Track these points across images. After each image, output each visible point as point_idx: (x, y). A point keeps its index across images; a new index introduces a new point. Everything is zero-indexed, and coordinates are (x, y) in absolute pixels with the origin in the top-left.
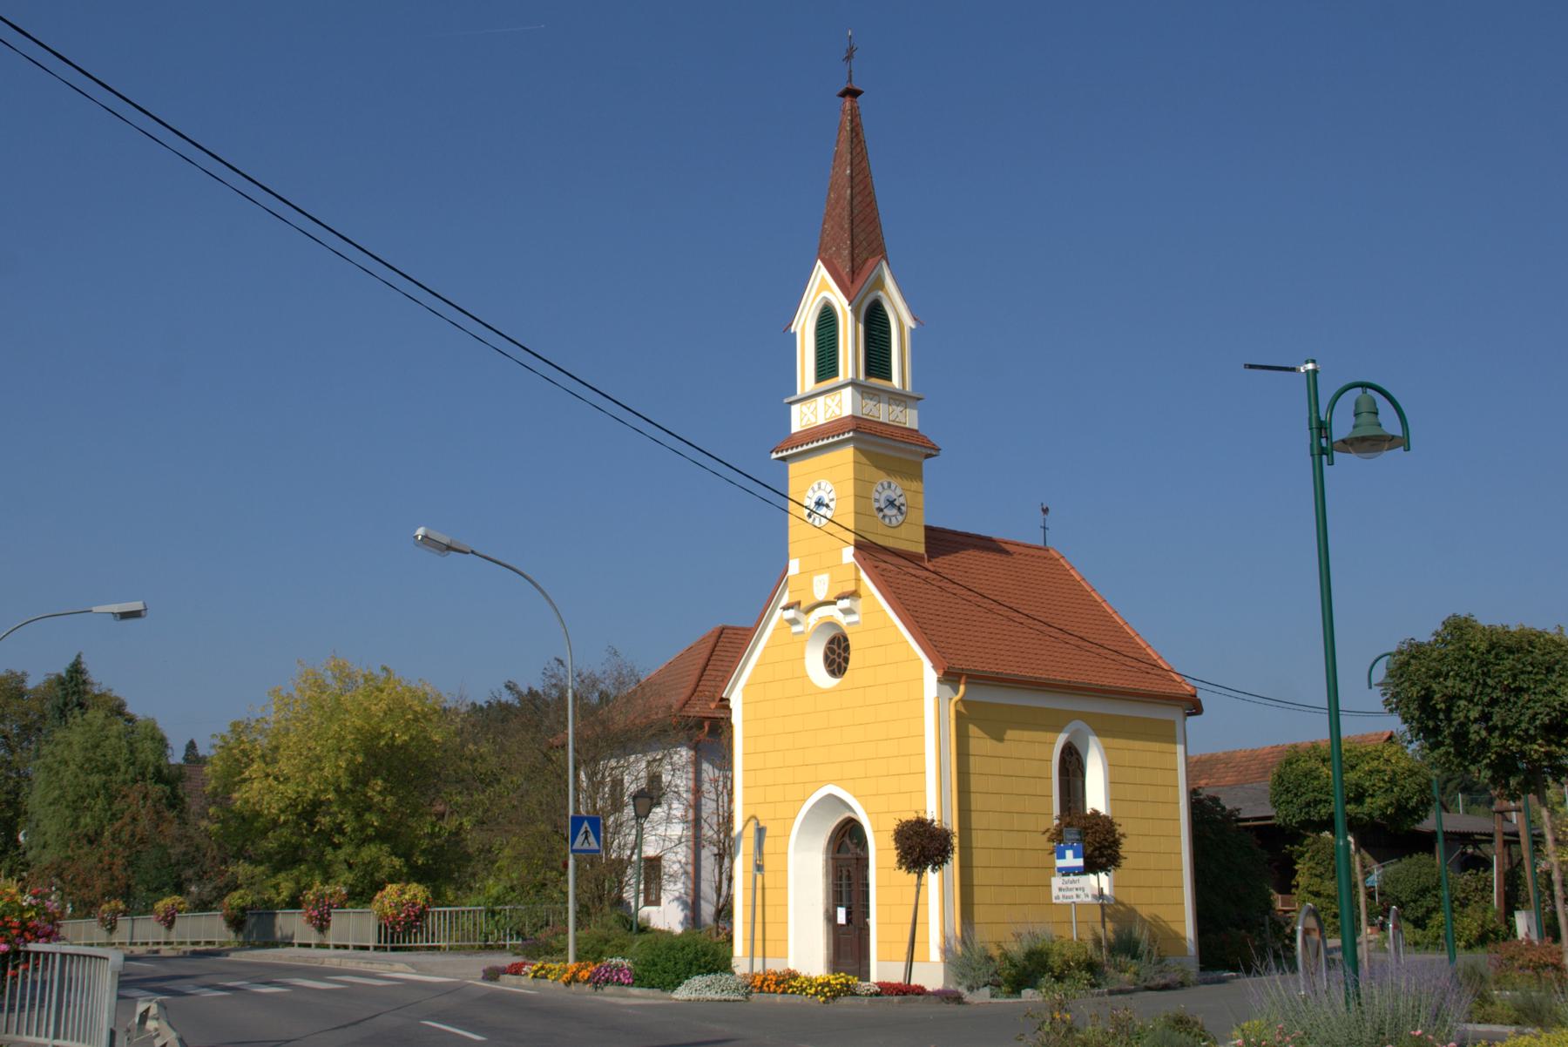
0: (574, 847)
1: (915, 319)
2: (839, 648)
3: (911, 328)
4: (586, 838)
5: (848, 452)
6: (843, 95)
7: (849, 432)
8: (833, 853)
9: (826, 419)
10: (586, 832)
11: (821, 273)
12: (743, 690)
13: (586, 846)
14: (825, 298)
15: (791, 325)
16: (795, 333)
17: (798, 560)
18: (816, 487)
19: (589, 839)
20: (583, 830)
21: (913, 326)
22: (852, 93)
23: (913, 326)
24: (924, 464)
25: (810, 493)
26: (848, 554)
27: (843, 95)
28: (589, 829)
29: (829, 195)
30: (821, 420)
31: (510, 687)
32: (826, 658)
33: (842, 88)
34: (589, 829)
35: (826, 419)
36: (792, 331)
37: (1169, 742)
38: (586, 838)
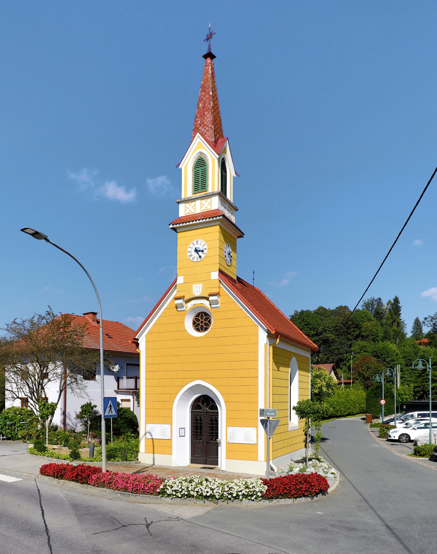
0: (105, 415)
1: (236, 173)
2: (202, 319)
3: (233, 176)
4: (110, 409)
5: (217, 229)
6: (205, 57)
7: (220, 216)
8: (192, 409)
9: (201, 211)
10: (110, 406)
11: (198, 140)
12: (146, 336)
13: (110, 414)
14: (201, 153)
15: (179, 164)
16: (181, 169)
17: (183, 277)
18: (195, 243)
19: (112, 409)
20: (109, 405)
21: (235, 176)
22: (210, 55)
23: (235, 176)
24: (237, 240)
25: (191, 246)
26: (215, 275)
27: (205, 57)
28: (111, 404)
29: (198, 104)
30: (198, 211)
31: (329, 308)
32: (194, 323)
33: (205, 52)
34: (111, 404)
35: (201, 211)
36: (180, 168)
37: (286, 367)
38: (110, 409)
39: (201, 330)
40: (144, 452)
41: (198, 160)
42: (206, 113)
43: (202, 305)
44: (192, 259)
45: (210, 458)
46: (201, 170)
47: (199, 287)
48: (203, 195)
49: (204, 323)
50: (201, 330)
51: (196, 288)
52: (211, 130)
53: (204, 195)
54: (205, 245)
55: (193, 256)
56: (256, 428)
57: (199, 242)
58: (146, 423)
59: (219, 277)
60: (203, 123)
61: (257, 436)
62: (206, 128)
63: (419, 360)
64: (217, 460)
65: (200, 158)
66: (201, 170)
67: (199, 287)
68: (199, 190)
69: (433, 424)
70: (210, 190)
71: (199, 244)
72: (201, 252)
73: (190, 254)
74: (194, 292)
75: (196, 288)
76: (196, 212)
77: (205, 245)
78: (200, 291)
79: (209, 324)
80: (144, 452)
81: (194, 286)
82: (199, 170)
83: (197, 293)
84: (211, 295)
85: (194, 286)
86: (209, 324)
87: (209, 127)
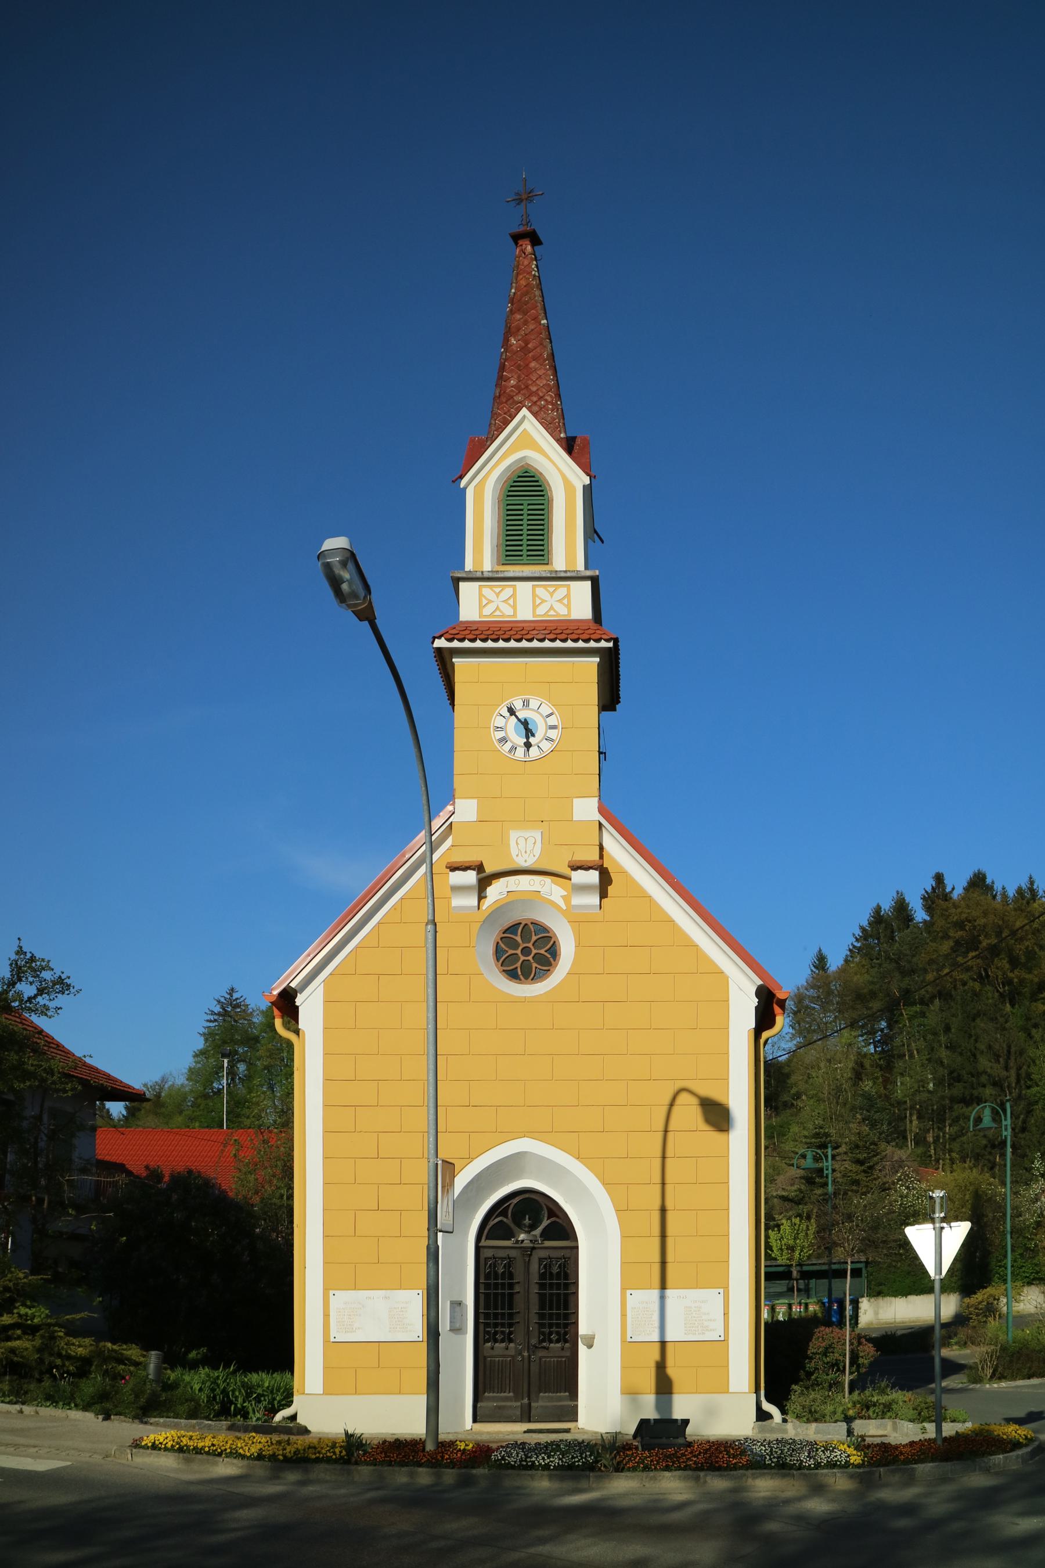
15: (461, 477)
17: (475, 801)
30: (525, 613)
32: (498, 952)
36: (462, 485)
39: (521, 977)
40: (747, 1391)
41: (519, 477)
42: (533, 364)
43: (534, 898)
44: (510, 751)
45: (489, 1399)
46: (529, 505)
47: (531, 841)
48: (544, 575)
49: (532, 955)
50: (521, 977)
51: (521, 841)
52: (552, 410)
53: (549, 575)
54: (552, 714)
55: (511, 741)
56: (721, 1291)
57: (534, 704)
58: (328, 1287)
59: (600, 811)
60: (527, 387)
61: (726, 1314)
62: (536, 401)
63: (986, 1106)
64: (572, 1403)
65: (526, 472)
66: (529, 505)
67: (531, 841)
68: (521, 556)
69: (785, 1289)
70: (559, 562)
71: (506, 723)
72: (525, 740)
73: (500, 735)
74: (514, 856)
75: (521, 841)
76: (519, 618)
77: (552, 714)
78: (537, 851)
79: (551, 960)
80: (747, 1391)
81: (514, 835)
82: (522, 505)
83: (525, 856)
84: (575, 868)
85: (514, 835)
86: (551, 960)
87: (546, 400)
